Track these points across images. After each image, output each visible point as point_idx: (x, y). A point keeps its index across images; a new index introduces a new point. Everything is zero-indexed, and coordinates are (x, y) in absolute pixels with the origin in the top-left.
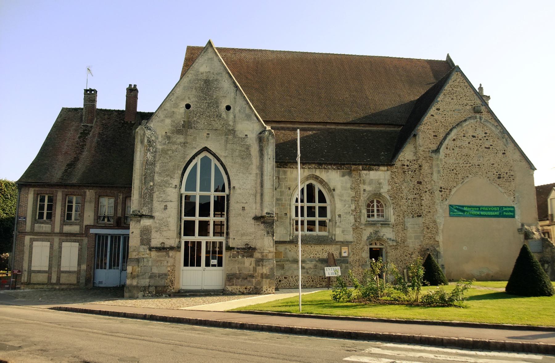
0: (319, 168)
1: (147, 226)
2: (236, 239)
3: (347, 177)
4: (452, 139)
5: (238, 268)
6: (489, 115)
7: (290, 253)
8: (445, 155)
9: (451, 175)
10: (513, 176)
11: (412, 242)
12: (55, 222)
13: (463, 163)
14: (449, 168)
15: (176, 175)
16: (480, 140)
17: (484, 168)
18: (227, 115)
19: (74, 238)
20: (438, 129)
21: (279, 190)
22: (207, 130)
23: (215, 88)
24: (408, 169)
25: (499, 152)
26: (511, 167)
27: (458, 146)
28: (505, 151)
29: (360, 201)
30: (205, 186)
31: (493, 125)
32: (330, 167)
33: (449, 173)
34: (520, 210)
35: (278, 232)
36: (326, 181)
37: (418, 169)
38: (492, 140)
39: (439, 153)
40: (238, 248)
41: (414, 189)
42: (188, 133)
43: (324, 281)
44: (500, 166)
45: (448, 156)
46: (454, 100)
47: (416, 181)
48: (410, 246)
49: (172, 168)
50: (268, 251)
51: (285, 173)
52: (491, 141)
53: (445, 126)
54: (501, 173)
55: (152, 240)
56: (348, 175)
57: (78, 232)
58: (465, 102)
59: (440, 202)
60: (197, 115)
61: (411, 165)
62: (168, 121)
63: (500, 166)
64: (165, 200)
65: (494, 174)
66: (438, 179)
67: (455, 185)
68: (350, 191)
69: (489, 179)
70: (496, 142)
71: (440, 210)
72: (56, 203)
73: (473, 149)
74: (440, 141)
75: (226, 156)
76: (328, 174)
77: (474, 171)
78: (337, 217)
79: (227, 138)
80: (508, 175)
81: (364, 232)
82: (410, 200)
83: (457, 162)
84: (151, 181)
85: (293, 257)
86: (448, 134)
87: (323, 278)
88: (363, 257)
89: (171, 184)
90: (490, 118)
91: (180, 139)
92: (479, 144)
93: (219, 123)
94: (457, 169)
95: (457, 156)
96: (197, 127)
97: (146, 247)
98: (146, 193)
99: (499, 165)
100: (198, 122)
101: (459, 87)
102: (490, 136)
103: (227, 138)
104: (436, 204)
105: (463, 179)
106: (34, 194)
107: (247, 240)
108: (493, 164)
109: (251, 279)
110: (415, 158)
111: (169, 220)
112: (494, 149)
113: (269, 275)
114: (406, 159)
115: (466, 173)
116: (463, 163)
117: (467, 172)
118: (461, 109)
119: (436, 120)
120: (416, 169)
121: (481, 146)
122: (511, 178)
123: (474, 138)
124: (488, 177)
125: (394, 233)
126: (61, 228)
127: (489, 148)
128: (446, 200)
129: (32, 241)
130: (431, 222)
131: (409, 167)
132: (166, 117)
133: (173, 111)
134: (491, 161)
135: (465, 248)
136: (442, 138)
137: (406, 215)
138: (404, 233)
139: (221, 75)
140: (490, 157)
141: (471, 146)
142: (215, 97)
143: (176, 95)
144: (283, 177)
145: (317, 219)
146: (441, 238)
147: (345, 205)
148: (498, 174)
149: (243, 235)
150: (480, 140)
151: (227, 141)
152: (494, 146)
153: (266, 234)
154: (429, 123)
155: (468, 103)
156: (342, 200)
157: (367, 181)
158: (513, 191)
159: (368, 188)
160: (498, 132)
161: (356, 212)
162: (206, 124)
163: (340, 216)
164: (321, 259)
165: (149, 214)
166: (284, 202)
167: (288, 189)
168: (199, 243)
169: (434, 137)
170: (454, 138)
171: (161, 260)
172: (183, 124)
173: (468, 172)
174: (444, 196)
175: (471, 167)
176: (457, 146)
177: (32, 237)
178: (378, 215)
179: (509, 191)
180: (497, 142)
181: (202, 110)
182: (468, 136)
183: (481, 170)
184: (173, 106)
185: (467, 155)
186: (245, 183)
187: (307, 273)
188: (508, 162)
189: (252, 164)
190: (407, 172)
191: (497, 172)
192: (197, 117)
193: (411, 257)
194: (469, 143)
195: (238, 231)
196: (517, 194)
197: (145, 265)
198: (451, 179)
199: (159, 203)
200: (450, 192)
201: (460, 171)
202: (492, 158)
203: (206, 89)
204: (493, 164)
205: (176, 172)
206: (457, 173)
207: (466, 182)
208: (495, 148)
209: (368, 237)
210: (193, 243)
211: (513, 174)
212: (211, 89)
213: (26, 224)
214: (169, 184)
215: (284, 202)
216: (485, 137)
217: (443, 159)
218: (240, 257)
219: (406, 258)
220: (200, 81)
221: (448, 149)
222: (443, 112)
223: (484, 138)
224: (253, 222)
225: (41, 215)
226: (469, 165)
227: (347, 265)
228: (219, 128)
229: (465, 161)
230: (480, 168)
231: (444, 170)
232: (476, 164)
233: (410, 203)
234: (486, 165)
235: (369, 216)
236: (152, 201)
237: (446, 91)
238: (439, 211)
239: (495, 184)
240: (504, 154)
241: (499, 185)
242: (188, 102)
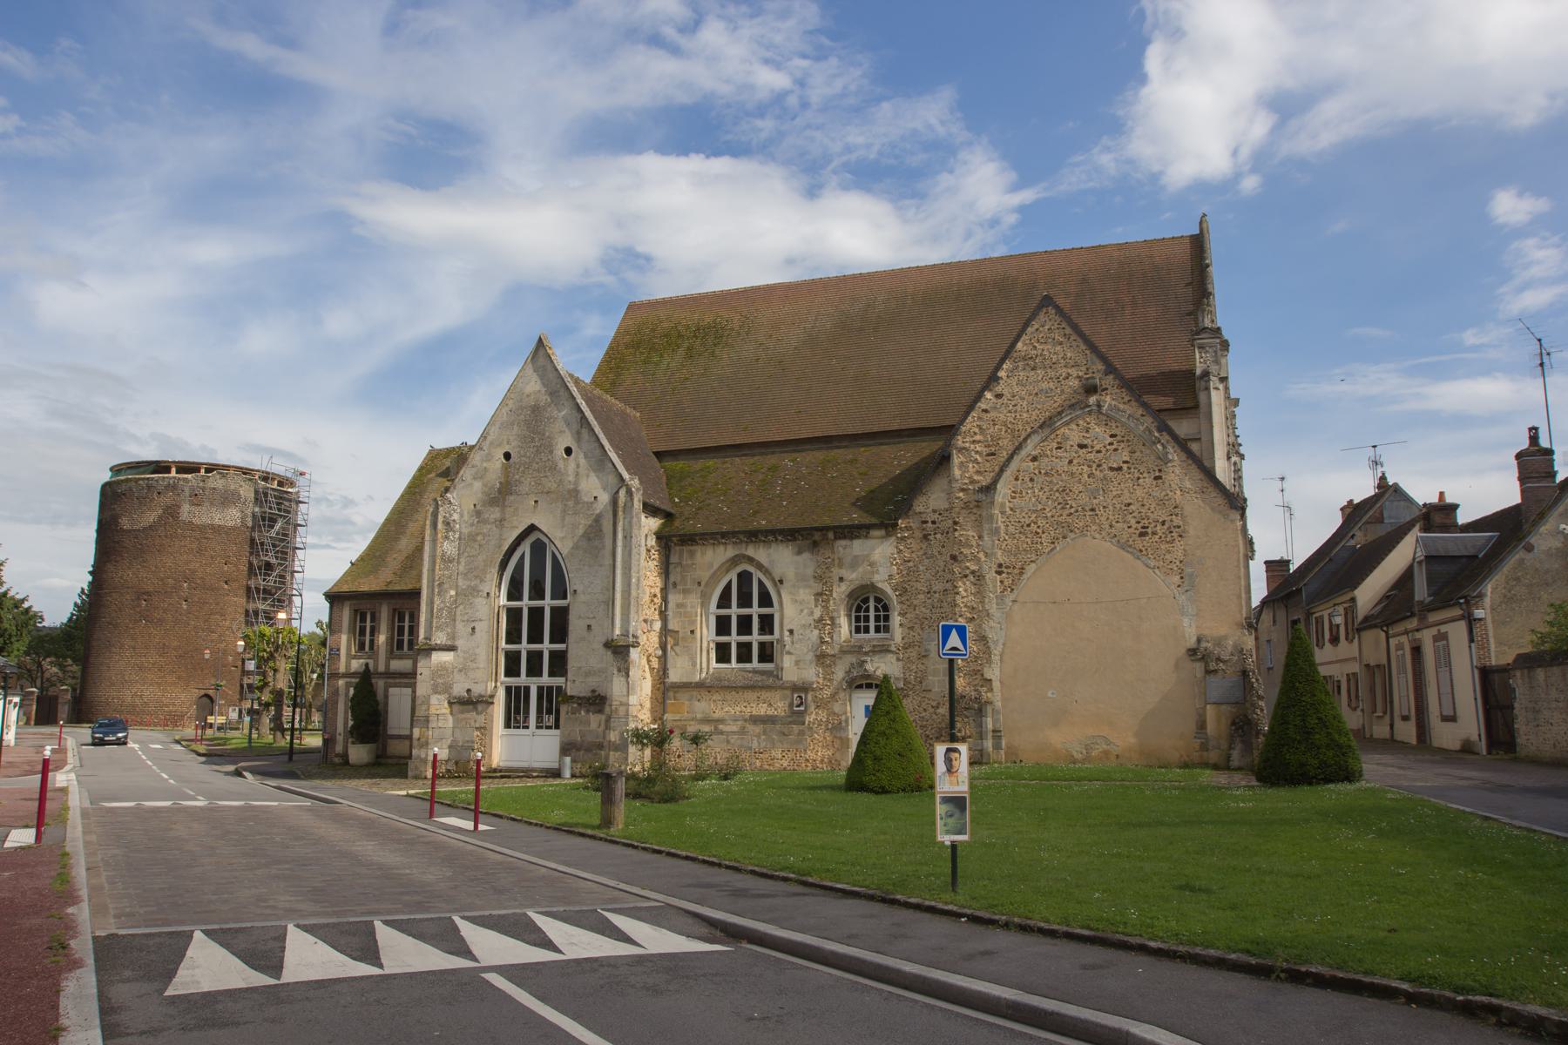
0: (752, 541)
1: (445, 663)
2: (577, 682)
3: (806, 556)
5: (580, 731)
6: (1124, 395)
16: (1099, 452)
28: (1160, 471)
32: (770, 538)
38: (1130, 449)
40: (579, 698)
42: (506, 504)
43: (757, 759)
49: (482, 564)
51: (692, 554)
54: (1149, 523)
62: (478, 485)
65: (1129, 527)
72: (379, 623)
73: (1081, 474)
76: (771, 551)
78: (787, 633)
79: (565, 505)
84: (451, 588)
86: (1019, 448)
87: (756, 753)
91: (495, 513)
97: (442, 697)
98: (442, 609)
105: (1053, 543)
108: (1129, 505)
109: (599, 752)
110: (947, 506)
111: (477, 651)
112: (1132, 470)
117: (1063, 527)
121: (1099, 466)
123: (1084, 450)
125: (900, 663)
126: (387, 665)
127: (1120, 469)
128: (1013, 590)
132: (475, 478)
133: (485, 468)
135: (1053, 694)
138: (923, 664)
140: (1122, 490)
142: (547, 434)
143: (489, 438)
144: (689, 562)
145: (755, 638)
146: (997, 672)
147: (802, 611)
148: (1141, 525)
149: (588, 674)
150: (1099, 452)
152: (1133, 464)
156: (796, 601)
158: (1178, 563)
162: (533, 483)
163: (791, 632)
166: (689, 609)
168: (527, 689)
170: (1034, 453)
171: (465, 719)
174: (1006, 583)
177: (348, 680)
178: (878, 630)
180: (1142, 452)
185: (1064, 490)
187: (728, 742)
188: (1166, 498)
189: (604, 547)
191: (1138, 522)
193: (935, 713)
194: (1070, 462)
198: (1025, 546)
200: (1021, 574)
202: (1126, 491)
204: (1129, 505)
206: (1038, 530)
210: (518, 688)
214: (478, 591)
215: (689, 609)
216: (1111, 444)
217: (1007, 504)
218: (583, 713)
219: (924, 714)
223: (1108, 447)
225: (400, 645)
229: (1059, 504)
230: (1097, 515)
231: (1008, 526)
234: (1111, 508)
242: (507, 448)
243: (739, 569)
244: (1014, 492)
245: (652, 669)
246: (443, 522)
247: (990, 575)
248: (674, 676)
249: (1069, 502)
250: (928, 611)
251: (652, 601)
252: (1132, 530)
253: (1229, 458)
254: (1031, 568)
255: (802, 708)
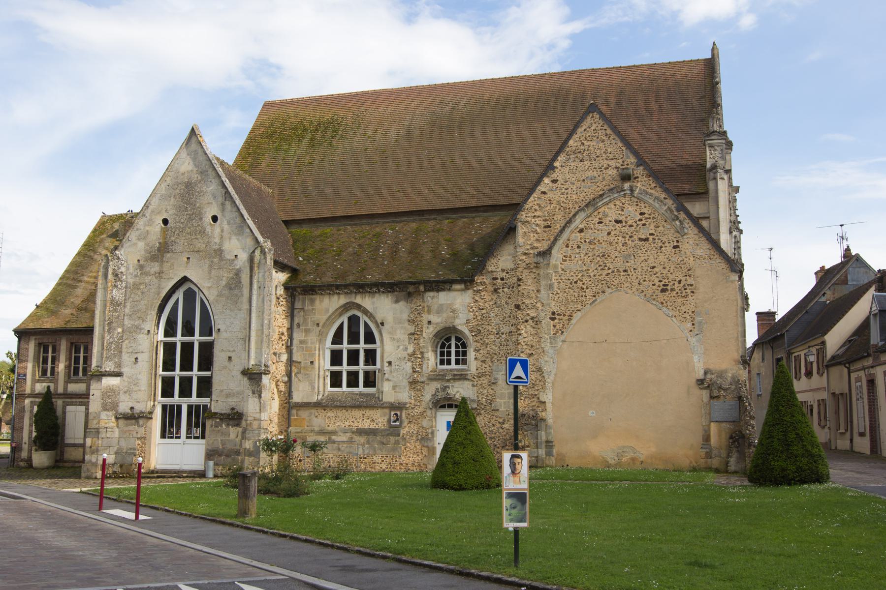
0: (360, 292)
1: (113, 386)
2: (219, 402)
3: (402, 304)
4: (578, 230)
7: (315, 419)
8: (564, 258)
9: (572, 291)
10: (692, 285)
11: (505, 403)
12: (58, 379)
13: (597, 269)
14: (569, 279)
15: (149, 317)
16: (631, 226)
17: (635, 274)
18: (213, 230)
19: (81, 400)
20: (554, 215)
21: (304, 328)
22: (186, 253)
23: (198, 192)
24: (503, 284)
25: (667, 244)
26: (689, 270)
27: (587, 241)
28: (678, 241)
29: (422, 340)
30: (189, 330)
31: (656, 198)
33: (569, 288)
34: (703, 346)
35: (301, 389)
36: (370, 310)
37: (516, 285)
38: (655, 224)
39: (550, 256)
41: (510, 317)
43: (362, 463)
44: (667, 270)
45: (568, 259)
46: (586, 163)
47: (514, 304)
48: (500, 410)
49: (144, 307)
50: (253, 419)
52: (652, 226)
53: (565, 208)
54: (669, 282)
55: (121, 404)
56: (405, 301)
57: (85, 392)
58: (605, 163)
59: (550, 337)
60: (176, 233)
61: (509, 278)
62: (141, 245)
63: (667, 270)
64: (136, 351)
65: (653, 285)
66: (548, 300)
67: (580, 307)
68: (406, 324)
69: (643, 294)
70: (661, 228)
71: (550, 351)
74: (556, 234)
75: (210, 287)
76: (375, 300)
77: (616, 282)
78: (387, 364)
79: (212, 261)
80: (682, 285)
81: (426, 387)
82: (504, 336)
83: (585, 268)
85: (319, 426)
86: (569, 222)
88: (425, 426)
89: (143, 329)
90: (653, 185)
91: (155, 267)
92: (627, 234)
93: (202, 242)
94: (584, 280)
95: (586, 258)
96: (175, 249)
98: (111, 343)
99: (664, 268)
100: (176, 243)
101: (595, 139)
102: (650, 218)
103: (212, 261)
104: (542, 340)
105: (594, 296)
106: (35, 344)
107: (233, 403)
108: (654, 267)
110: (512, 267)
111: (140, 377)
112: (657, 241)
113: (253, 451)
114: (500, 269)
115: (601, 286)
116: (597, 269)
118: (597, 176)
119: (550, 200)
120: (514, 284)
121: (631, 237)
122: (688, 290)
124: (643, 291)
126: (65, 388)
127: (647, 239)
128: (563, 332)
129: (65, 405)
130: (535, 370)
131: (505, 281)
132: (139, 239)
134: (649, 262)
135: (593, 413)
136: (559, 229)
137: (496, 361)
138: (492, 389)
139: (206, 173)
141: (611, 238)
142: (198, 205)
143: (151, 207)
144: (310, 308)
146: (550, 396)
147: (398, 347)
148: (663, 283)
149: (228, 396)
150: (631, 226)
151: (211, 267)
152: (657, 236)
153: (251, 394)
154: (537, 207)
155: (611, 165)
157: (435, 307)
158: (690, 313)
159: (435, 319)
160: (666, 210)
161: (417, 356)
162: (186, 244)
163: (390, 363)
164: (361, 429)
165: (116, 370)
166: (309, 345)
167: (315, 326)
168: (179, 407)
169: (545, 229)
172: (158, 248)
173: (605, 285)
174: (558, 327)
175: (610, 275)
176: (585, 242)
179: (683, 312)
180: (664, 227)
181: (182, 226)
182: (607, 222)
183: (629, 280)
184: (147, 223)
185: (603, 256)
186: (233, 323)
187: (339, 449)
189: (242, 295)
190: (501, 290)
192: (176, 236)
194: (609, 234)
195: (222, 391)
196: (698, 319)
197: (108, 436)
199: (128, 355)
200: (570, 320)
201: (590, 283)
203: (187, 195)
204: (654, 267)
205: (149, 313)
206: (583, 286)
207: (600, 302)
208: (659, 239)
209: (432, 395)
210: (172, 406)
211: (693, 282)
212: (193, 195)
213: (25, 384)
214: (141, 329)
215: (309, 345)
216: (640, 220)
218: (224, 426)
220: (180, 185)
221: (570, 248)
222: (563, 184)
223: (638, 223)
224: (240, 377)
226: (605, 272)
227: (397, 438)
228: (202, 248)
229: (599, 266)
230: (629, 275)
231: (559, 282)
232: (621, 270)
233: (505, 341)
234: (640, 270)
235: (442, 362)
236: (121, 352)
237: (570, 148)
238: (548, 352)
239: (654, 302)
240: (675, 247)
241: (662, 303)
243: (350, 314)
244: (565, 256)
245: (279, 392)
246: (113, 273)
247: (546, 321)
248: (297, 398)
249: (607, 265)
250: (496, 348)
251: (281, 338)
252: (655, 287)
253: (731, 232)
254: (577, 316)
255: (398, 423)
